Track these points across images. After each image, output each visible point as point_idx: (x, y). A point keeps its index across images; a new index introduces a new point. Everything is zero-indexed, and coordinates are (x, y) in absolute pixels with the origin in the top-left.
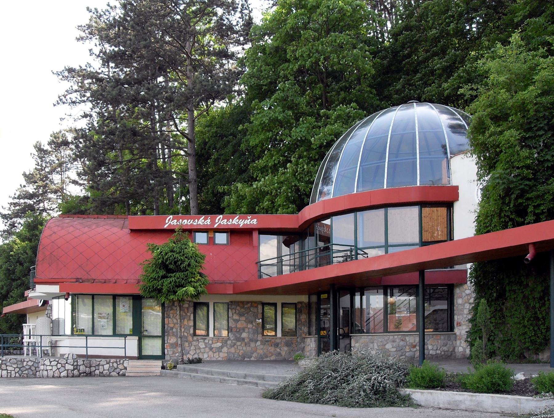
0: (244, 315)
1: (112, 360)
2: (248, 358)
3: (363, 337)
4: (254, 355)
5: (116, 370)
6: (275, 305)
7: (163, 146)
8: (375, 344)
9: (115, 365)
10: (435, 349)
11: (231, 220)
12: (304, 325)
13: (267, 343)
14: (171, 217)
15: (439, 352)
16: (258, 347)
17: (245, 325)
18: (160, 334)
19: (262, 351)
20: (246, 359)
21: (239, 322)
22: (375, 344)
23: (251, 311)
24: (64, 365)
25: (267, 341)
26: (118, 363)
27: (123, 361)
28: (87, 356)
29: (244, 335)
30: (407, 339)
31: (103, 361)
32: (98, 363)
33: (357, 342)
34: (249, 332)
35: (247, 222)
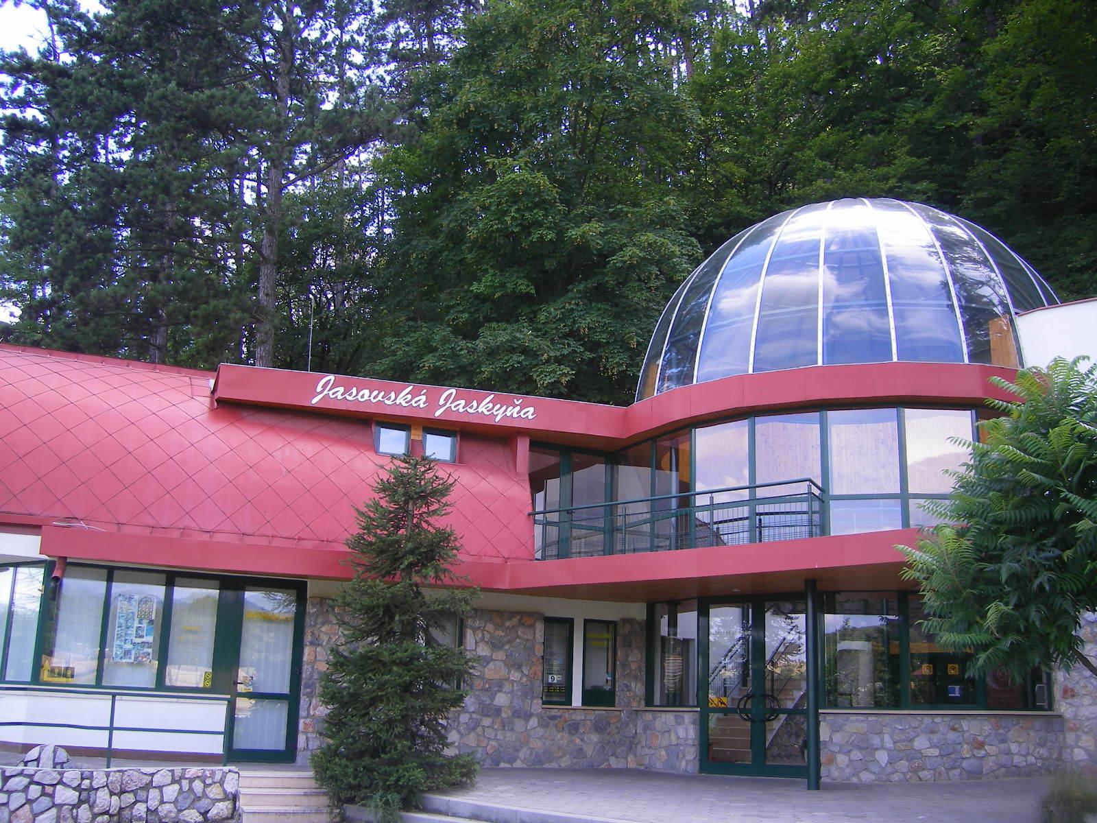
0: (501, 648)
1: (193, 770)
2: (509, 761)
3: (853, 718)
4: (521, 755)
5: (198, 804)
6: (569, 622)
7: (383, 193)
8: (887, 738)
9: (198, 786)
10: (1023, 752)
11: (475, 403)
12: (636, 678)
13: (552, 723)
14: (332, 377)
15: (1031, 759)
16: (532, 733)
17: (503, 672)
18: (286, 690)
19: (540, 744)
20: (502, 765)
21: (491, 665)
22: (887, 738)
23: (518, 637)
24: (49, 790)
25: (553, 718)
26: (209, 781)
27: (224, 775)
28: (109, 754)
29: (501, 699)
30: (965, 724)
31: (162, 774)
32: (147, 779)
33: (837, 729)
34: (511, 692)
35: (513, 412)
